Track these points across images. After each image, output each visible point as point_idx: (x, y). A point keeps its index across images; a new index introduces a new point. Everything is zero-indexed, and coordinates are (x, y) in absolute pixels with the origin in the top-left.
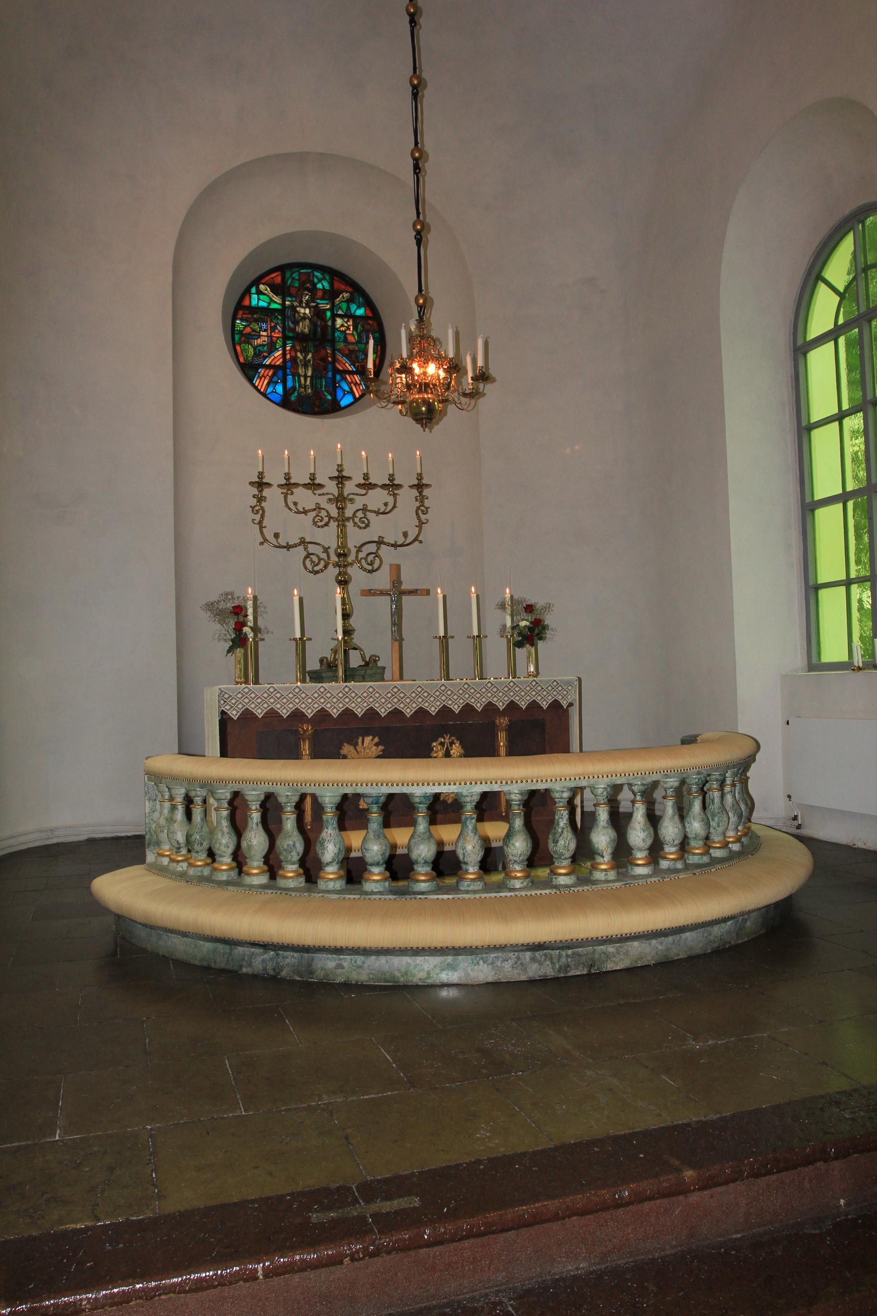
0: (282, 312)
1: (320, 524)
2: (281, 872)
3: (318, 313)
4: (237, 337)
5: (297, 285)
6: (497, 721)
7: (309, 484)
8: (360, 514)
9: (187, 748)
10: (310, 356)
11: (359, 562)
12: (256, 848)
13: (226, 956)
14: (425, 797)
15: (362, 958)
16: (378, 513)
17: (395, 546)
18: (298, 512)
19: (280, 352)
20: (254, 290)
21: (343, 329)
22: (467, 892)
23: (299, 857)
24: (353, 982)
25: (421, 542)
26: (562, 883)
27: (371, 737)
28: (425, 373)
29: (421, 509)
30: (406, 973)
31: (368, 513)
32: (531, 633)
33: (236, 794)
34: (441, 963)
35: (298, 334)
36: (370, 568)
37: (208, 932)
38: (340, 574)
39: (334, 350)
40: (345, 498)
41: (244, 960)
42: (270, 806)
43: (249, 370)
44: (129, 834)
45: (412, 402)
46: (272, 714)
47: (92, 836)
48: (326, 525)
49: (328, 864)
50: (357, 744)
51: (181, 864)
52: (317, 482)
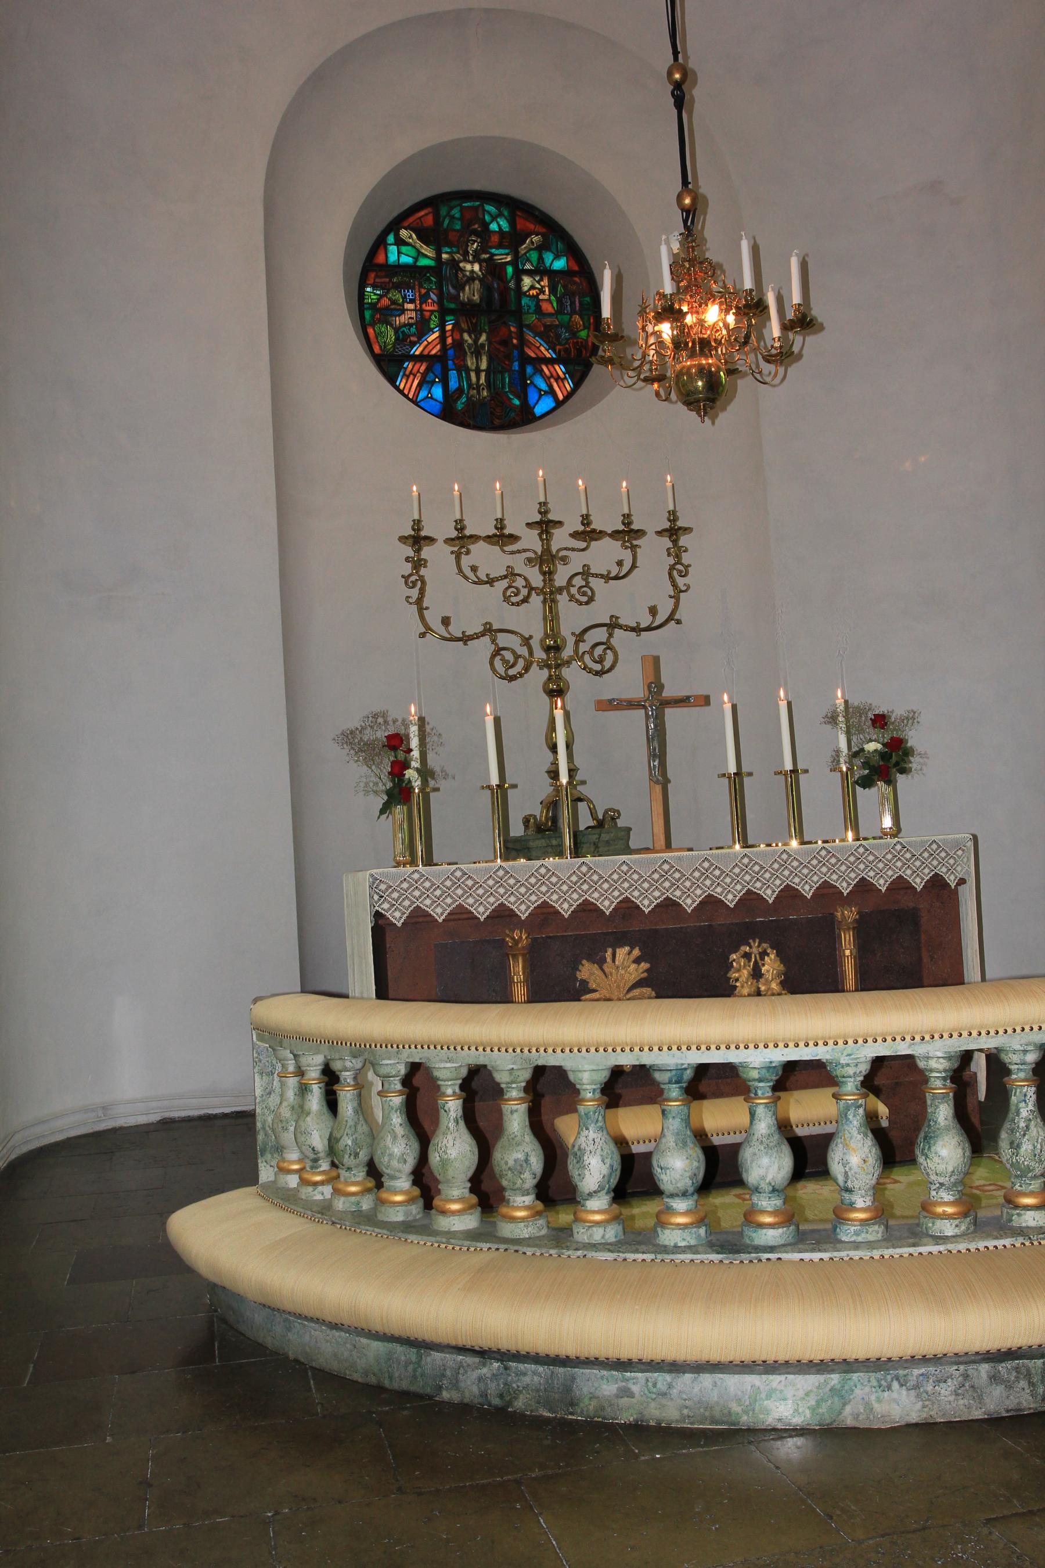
0: (437, 270)
1: (514, 599)
2: (504, 1210)
3: (493, 269)
4: (368, 314)
5: (458, 227)
6: (839, 914)
7: (495, 535)
8: (578, 581)
9: (317, 981)
10: (483, 338)
11: (581, 659)
12: (456, 1164)
13: (411, 1368)
14: (768, 1068)
15: (668, 1377)
16: (607, 578)
17: (637, 630)
18: (479, 582)
19: (436, 335)
20: (391, 238)
21: (534, 292)
22: (856, 1246)
23: (535, 1182)
24: (652, 1423)
25: (679, 622)
26: (1032, 1223)
27: (627, 948)
28: (701, 322)
29: (678, 569)
30: (749, 1409)
31: (591, 579)
32: (886, 761)
33: (415, 1067)
34: (819, 1387)
35: (463, 304)
36: (597, 667)
37: (378, 1328)
38: (550, 678)
39: (521, 326)
40: (553, 557)
41: (444, 1375)
42: (478, 1087)
43: (389, 364)
44: (227, 1110)
45: (679, 375)
46: (461, 915)
47: (167, 1115)
48: (525, 600)
49: (590, 1195)
50: (604, 960)
51: (320, 1188)
52: (507, 532)
